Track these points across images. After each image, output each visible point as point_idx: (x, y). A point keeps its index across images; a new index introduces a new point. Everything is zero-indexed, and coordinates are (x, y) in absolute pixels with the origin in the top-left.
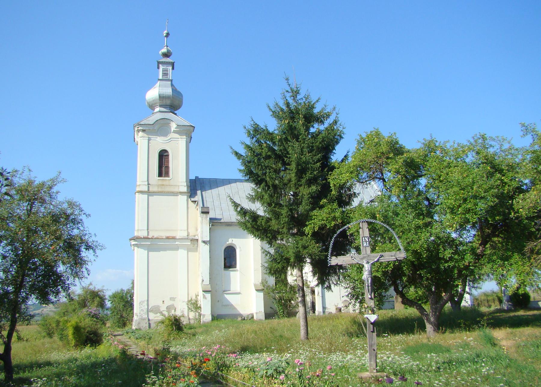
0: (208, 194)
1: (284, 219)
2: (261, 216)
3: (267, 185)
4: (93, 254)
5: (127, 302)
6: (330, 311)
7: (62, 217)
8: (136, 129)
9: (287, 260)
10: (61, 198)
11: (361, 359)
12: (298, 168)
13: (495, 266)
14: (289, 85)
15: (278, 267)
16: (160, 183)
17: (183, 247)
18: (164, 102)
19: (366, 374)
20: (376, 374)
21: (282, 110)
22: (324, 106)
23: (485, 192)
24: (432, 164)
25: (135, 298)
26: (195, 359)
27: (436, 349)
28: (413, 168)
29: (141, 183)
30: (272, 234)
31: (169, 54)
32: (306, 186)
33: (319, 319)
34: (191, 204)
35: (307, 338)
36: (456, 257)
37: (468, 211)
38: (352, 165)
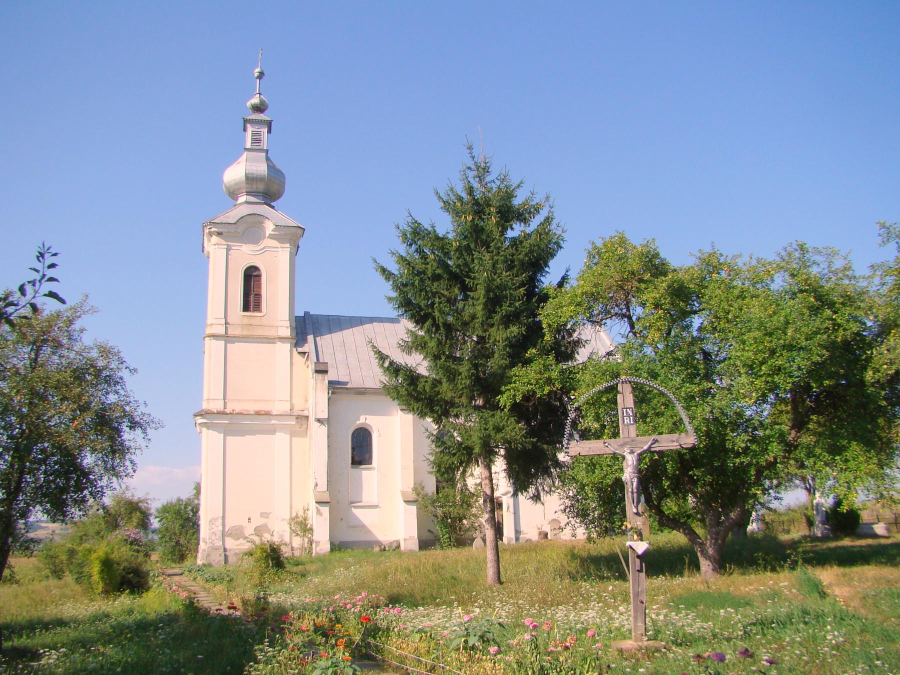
0: (325, 341)
1: (464, 381)
2: (423, 376)
3: (435, 324)
4: (143, 435)
5: (188, 519)
6: (528, 537)
7: (89, 374)
8: (207, 231)
9: (469, 450)
10: (87, 340)
11: (620, 616)
12: (489, 295)
13: (819, 464)
14: (473, 157)
15: (451, 460)
16: (246, 321)
17: (283, 428)
18: (255, 187)
19: (628, 644)
20: (646, 643)
21: (460, 199)
22: (529, 194)
23: (807, 339)
24: (713, 291)
25: (202, 513)
26: (318, 616)
27: (723, 600)
28: (682, 298)
29: (214, 322)
30: (441, 406)
31: (263, 107)
32: (501, 327)
33: (513, 550)
34: (298, 358)
35: (501, 583)
36: (754, 447)
37: (778, 370)
38: (580, 291)
